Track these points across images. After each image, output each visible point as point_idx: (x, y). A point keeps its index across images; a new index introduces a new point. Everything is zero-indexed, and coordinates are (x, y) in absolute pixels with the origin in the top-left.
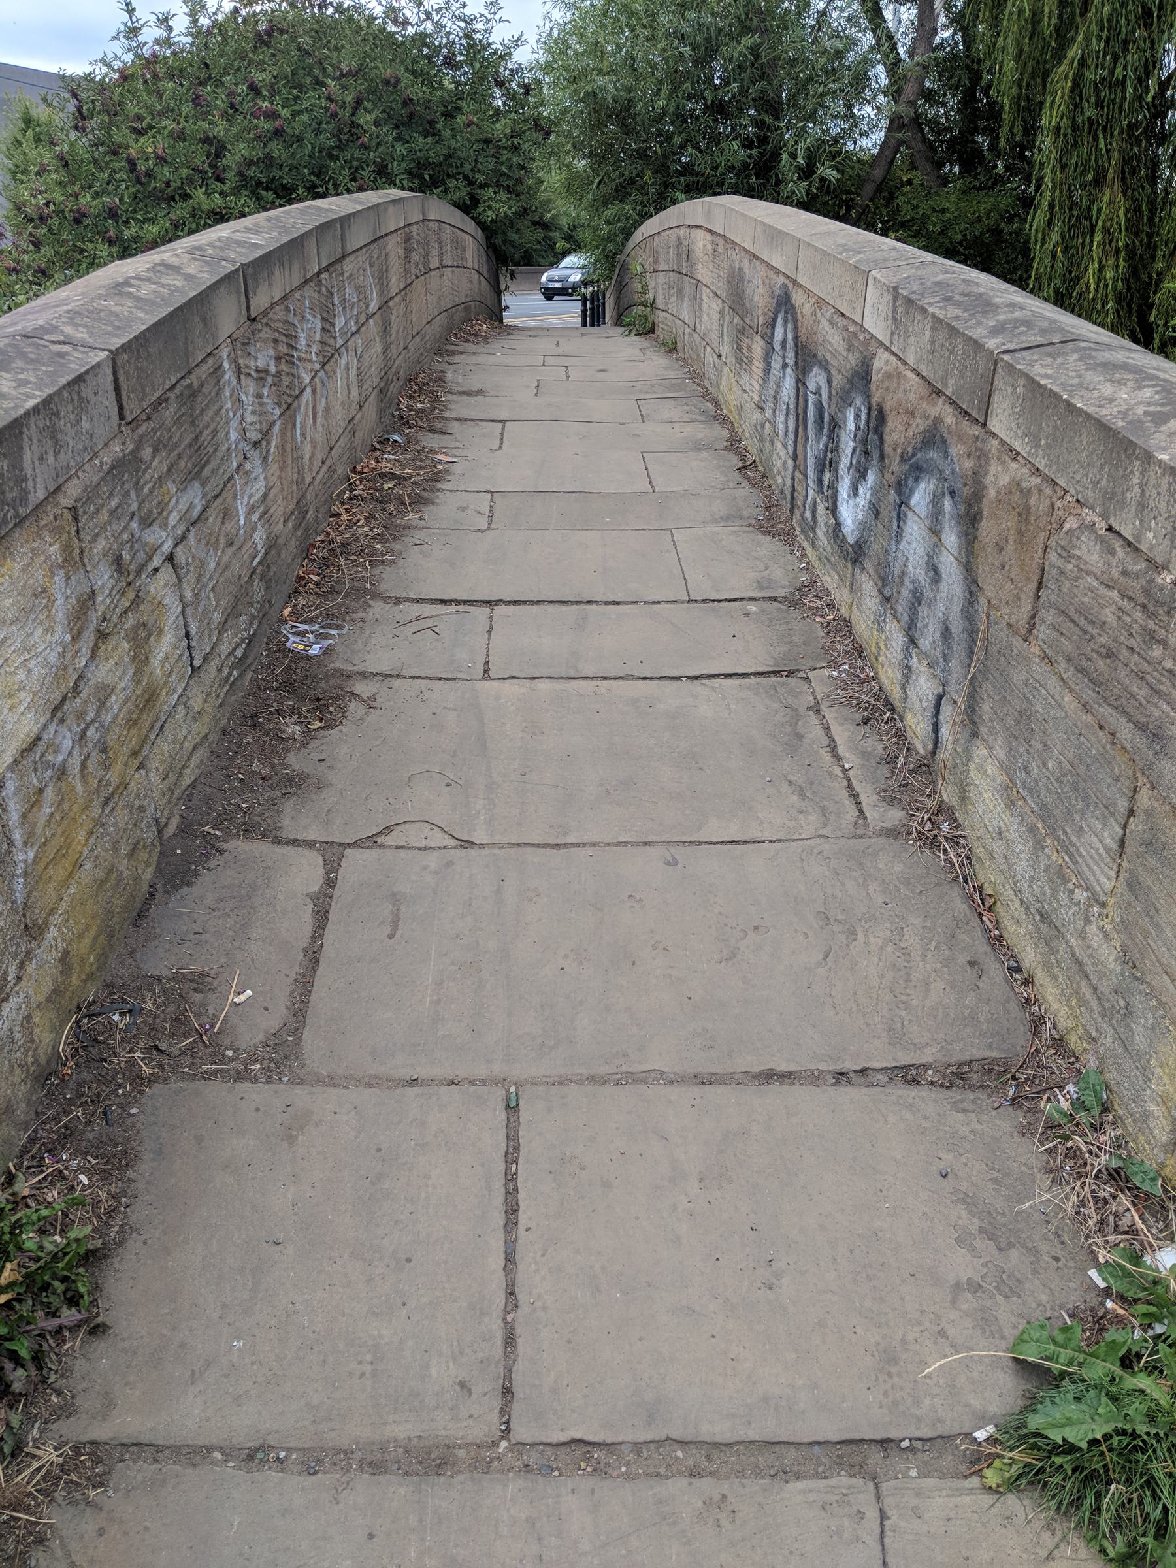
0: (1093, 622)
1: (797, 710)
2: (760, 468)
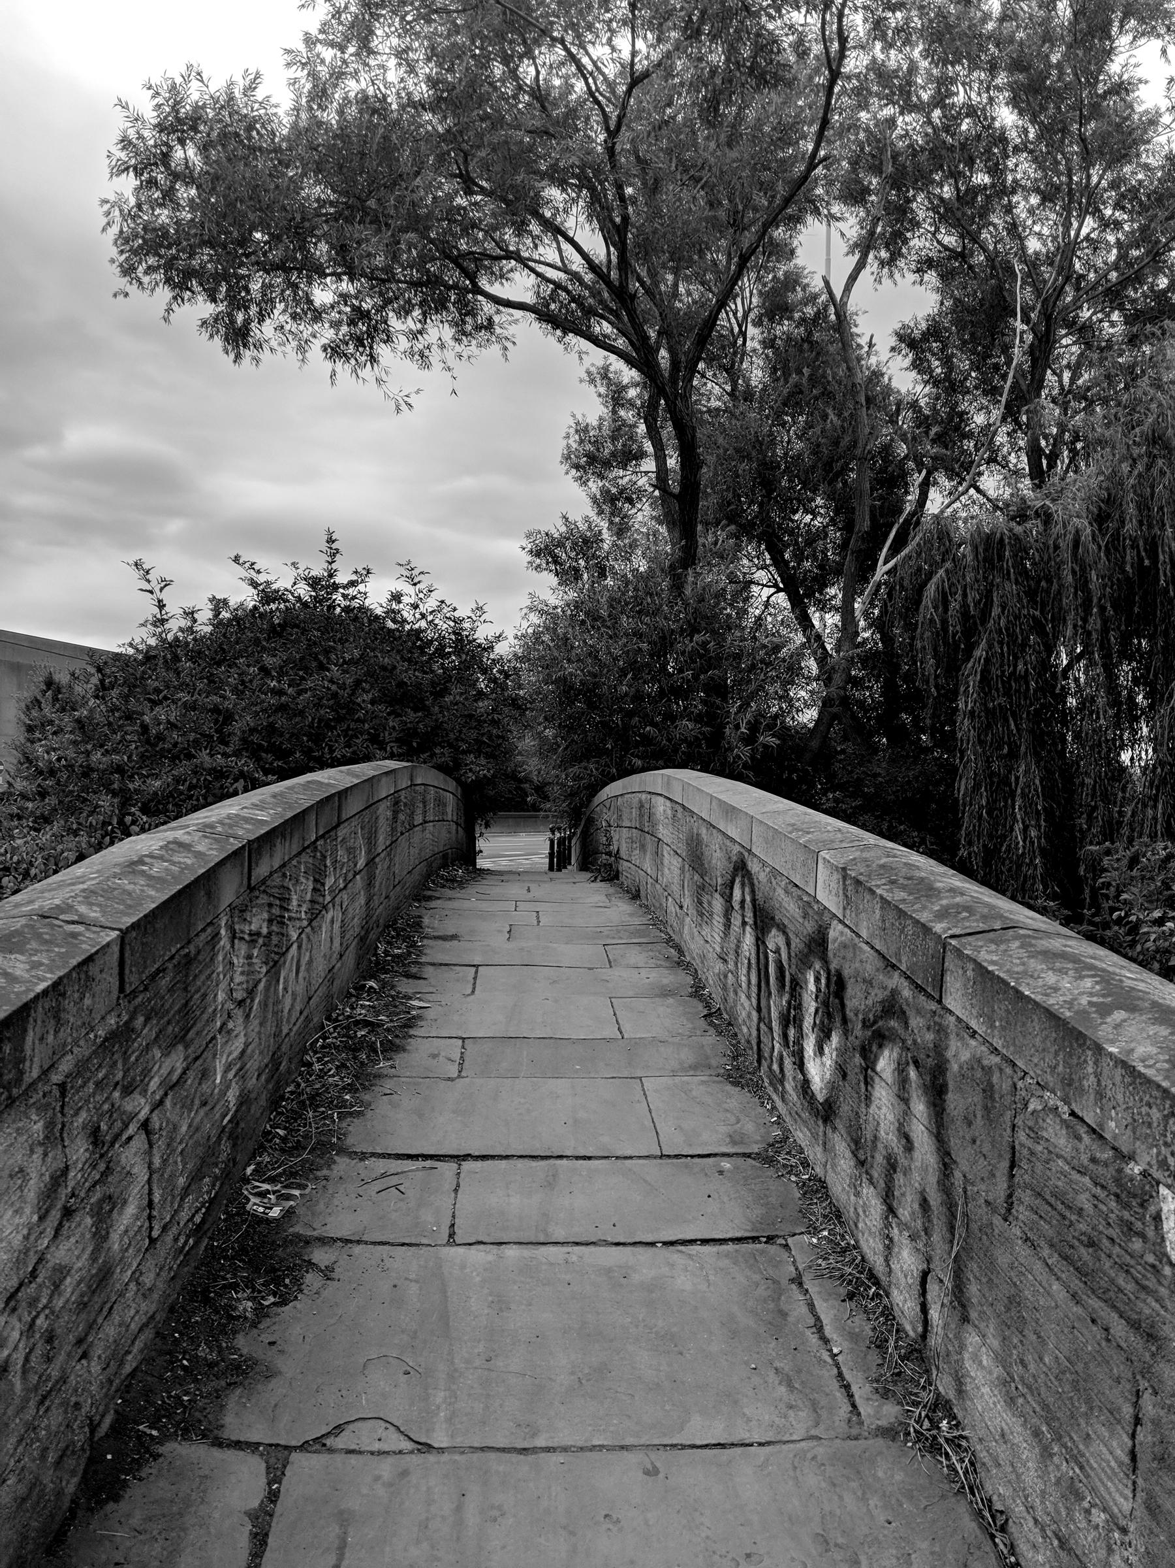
0: (1070, 1208)
1: (778, 1283)
2: (725, 1016)
